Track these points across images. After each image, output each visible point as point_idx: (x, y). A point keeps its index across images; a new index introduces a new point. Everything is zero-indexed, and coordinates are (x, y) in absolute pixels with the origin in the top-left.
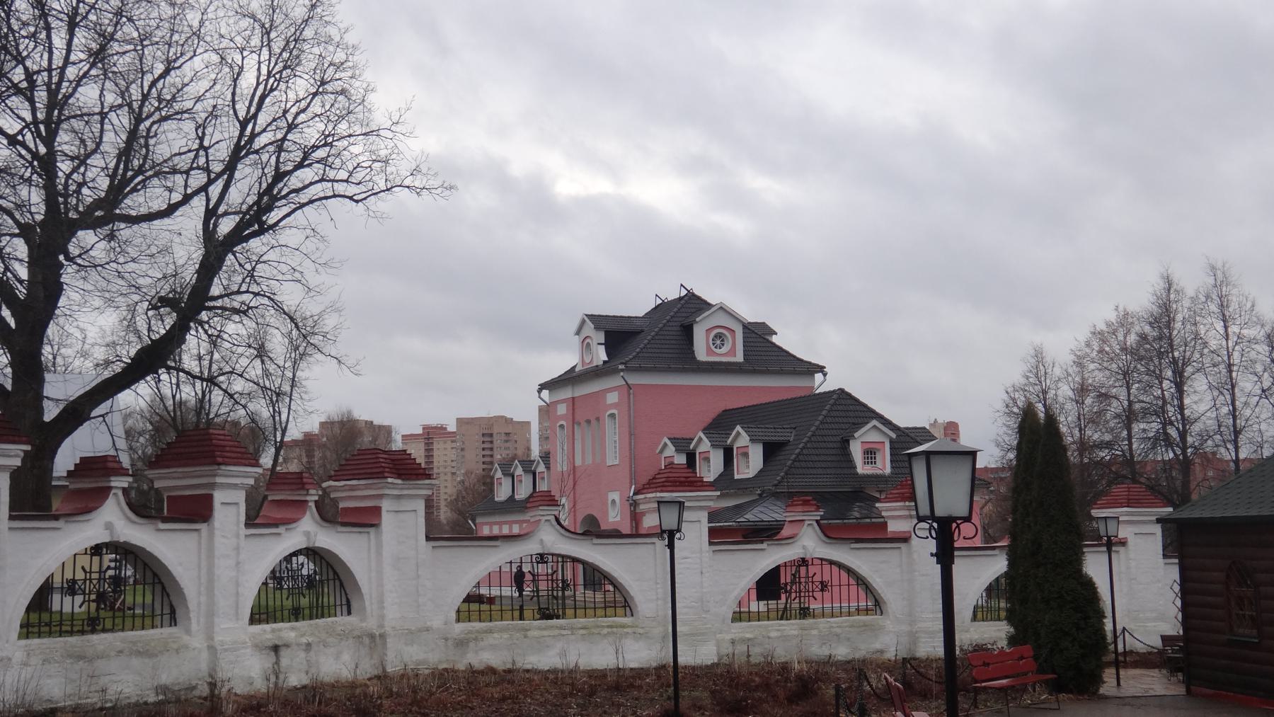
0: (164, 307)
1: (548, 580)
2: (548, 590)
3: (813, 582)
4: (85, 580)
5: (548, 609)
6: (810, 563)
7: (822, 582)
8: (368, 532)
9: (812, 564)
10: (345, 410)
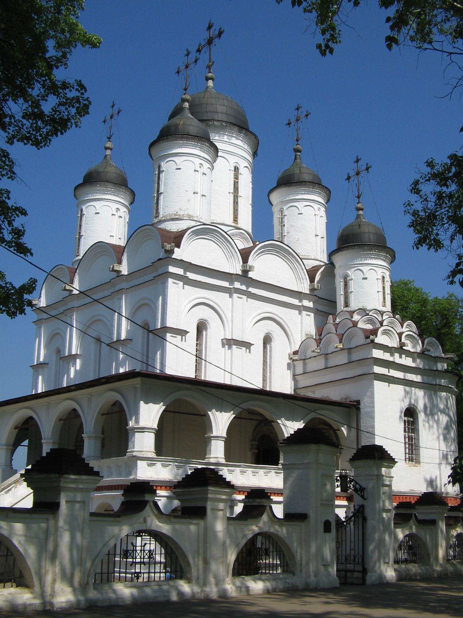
8: (198, 524)
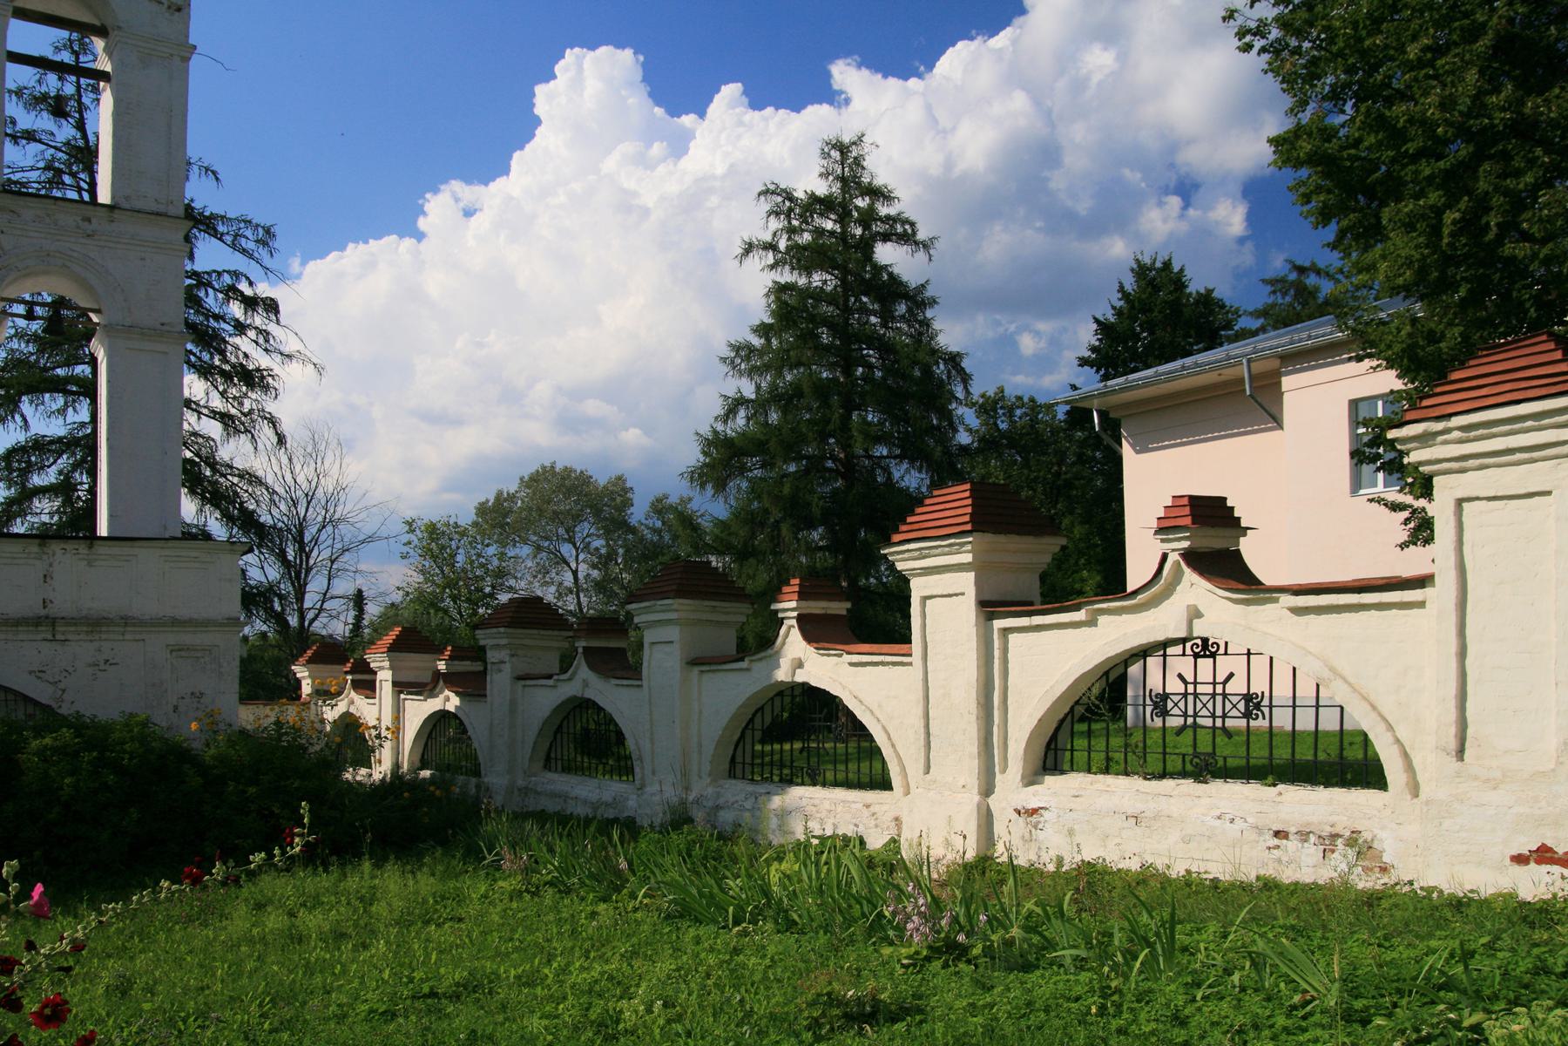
0: (882, 457)
1: (1195, 683)
2: (1214, 683)
3: (1225, 695)
4: (1185, 695)
5: (407, 594)
6: (1222, 651)
7: (1248, 698)
9: (1226, 654)
10: (548, 464)
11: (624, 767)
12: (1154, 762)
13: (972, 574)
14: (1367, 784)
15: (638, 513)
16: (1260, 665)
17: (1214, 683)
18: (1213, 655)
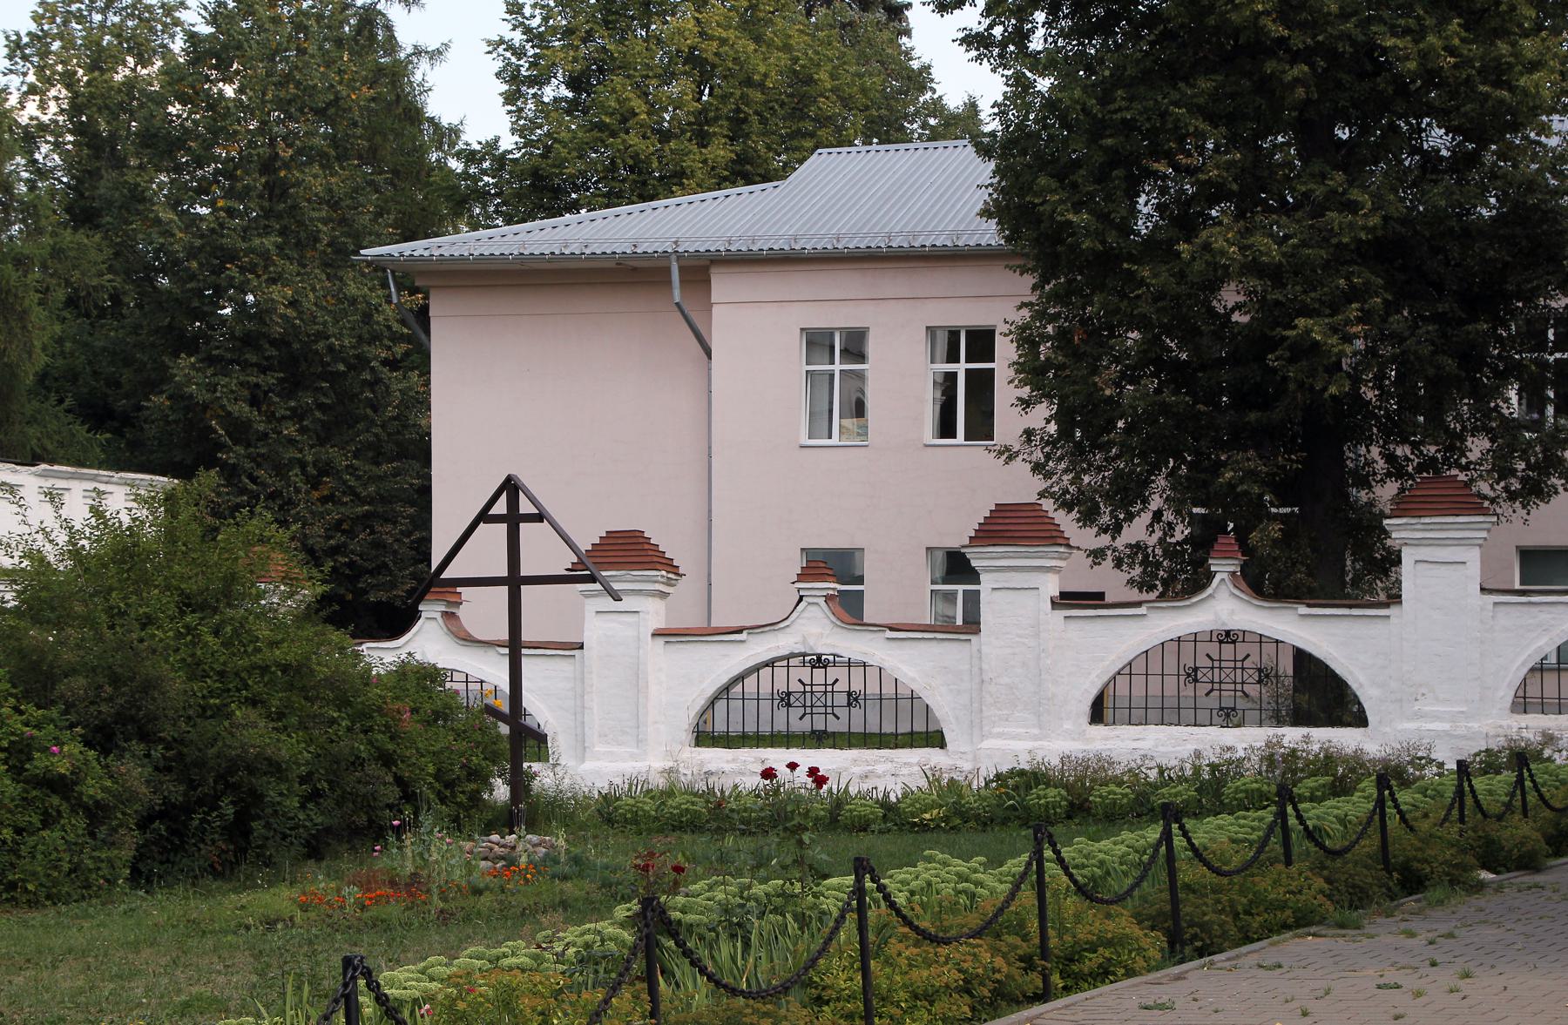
3: (804, 706)
7: (789, 705)
11: (1361, 720)
12: (1188, 714)
13: (505, 526)
14: (1358, 726)
15: (1004, 1004)
16: (872, 675)
17: (812, 714)
18: (1221, 709)
